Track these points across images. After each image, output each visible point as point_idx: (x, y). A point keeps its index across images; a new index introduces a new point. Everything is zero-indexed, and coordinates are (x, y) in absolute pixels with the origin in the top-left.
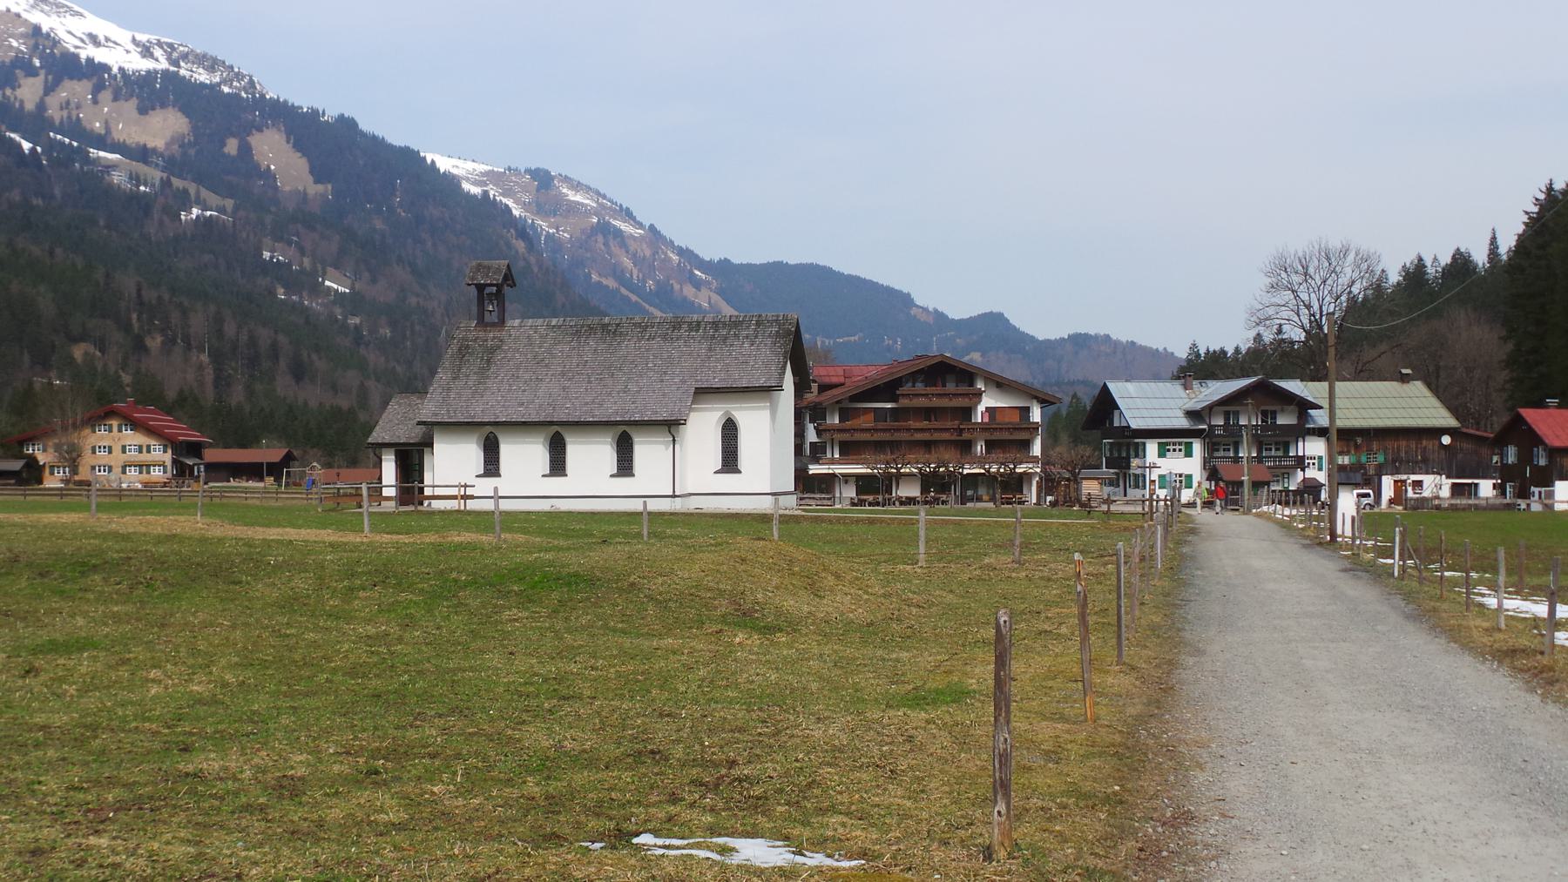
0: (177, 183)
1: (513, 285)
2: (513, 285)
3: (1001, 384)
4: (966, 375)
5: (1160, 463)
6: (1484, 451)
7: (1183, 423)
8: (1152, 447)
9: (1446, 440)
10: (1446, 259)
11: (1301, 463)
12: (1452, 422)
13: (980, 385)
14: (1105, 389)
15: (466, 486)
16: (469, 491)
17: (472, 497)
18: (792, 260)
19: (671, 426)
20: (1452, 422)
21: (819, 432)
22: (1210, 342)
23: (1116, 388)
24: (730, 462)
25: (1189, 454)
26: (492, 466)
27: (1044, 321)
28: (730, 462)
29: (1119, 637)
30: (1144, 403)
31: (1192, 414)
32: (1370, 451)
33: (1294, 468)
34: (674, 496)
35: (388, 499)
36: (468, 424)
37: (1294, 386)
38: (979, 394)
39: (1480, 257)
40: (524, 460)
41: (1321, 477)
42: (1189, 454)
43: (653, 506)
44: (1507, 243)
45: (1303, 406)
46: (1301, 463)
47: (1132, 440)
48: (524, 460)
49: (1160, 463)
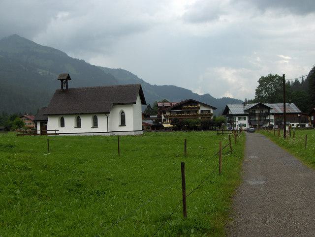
0: (51, 74)
1: (70, 79)
2: (70, 79)
3: (204, 105)
4: (196, 103)
5: (238, 122)
6: (307, 116)
7: (243, 113)
8: (237, 118)
9: (299, 115)
10: (294, 81)
11: (269, 121)
12: (300, 111)
13: (199, 105)
14: (227, 106)
15: (56, 130)
16: (57, 132)
17: (58, 134)
18: (168, 84)
19: (106, 113)
20: (300, 111)
21: (164, 116)
22: (250, 99)
23: (229, 106)
24: (123, 123)
25: (245, 120)
26: (62, 125)
27: (218, 95)
28: (123, 123)
29: (119, 151)
30: (234, 109)
31: (245, 111)
32: (283, 118)
33: (267, 122)
34: (108, 132)
35: (39, 134)
36: (56, 115)
37: (267, 105)
38: (199, 108)
39: (300, 81)
40: (70, 123)
41: (273, 124)
42: (245, 120)
43: (103, 134)
44: (305, 78)
45: (269, 108)
46: (269, 121)
47: (233, 116)
48: (70, 123)
49: (238, 122)
